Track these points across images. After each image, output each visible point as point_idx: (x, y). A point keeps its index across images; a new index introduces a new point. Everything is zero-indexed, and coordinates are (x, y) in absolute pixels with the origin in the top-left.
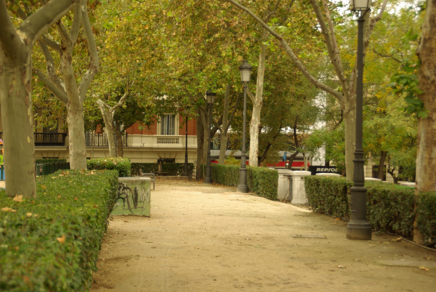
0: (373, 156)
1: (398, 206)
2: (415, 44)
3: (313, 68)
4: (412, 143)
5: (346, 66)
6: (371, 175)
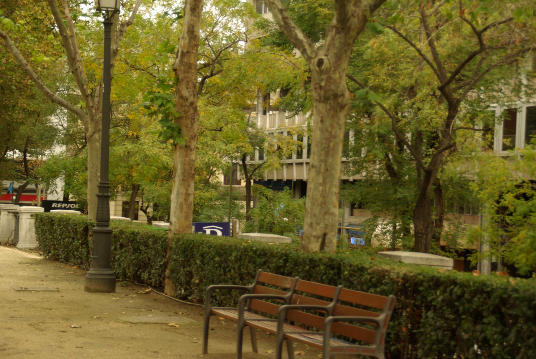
0: (123, 190)
1: (149, 250)
2: (173, 58)
3: (49, 77)
4: (170, 176)
5: (92, 78)
6: (120, 213)
